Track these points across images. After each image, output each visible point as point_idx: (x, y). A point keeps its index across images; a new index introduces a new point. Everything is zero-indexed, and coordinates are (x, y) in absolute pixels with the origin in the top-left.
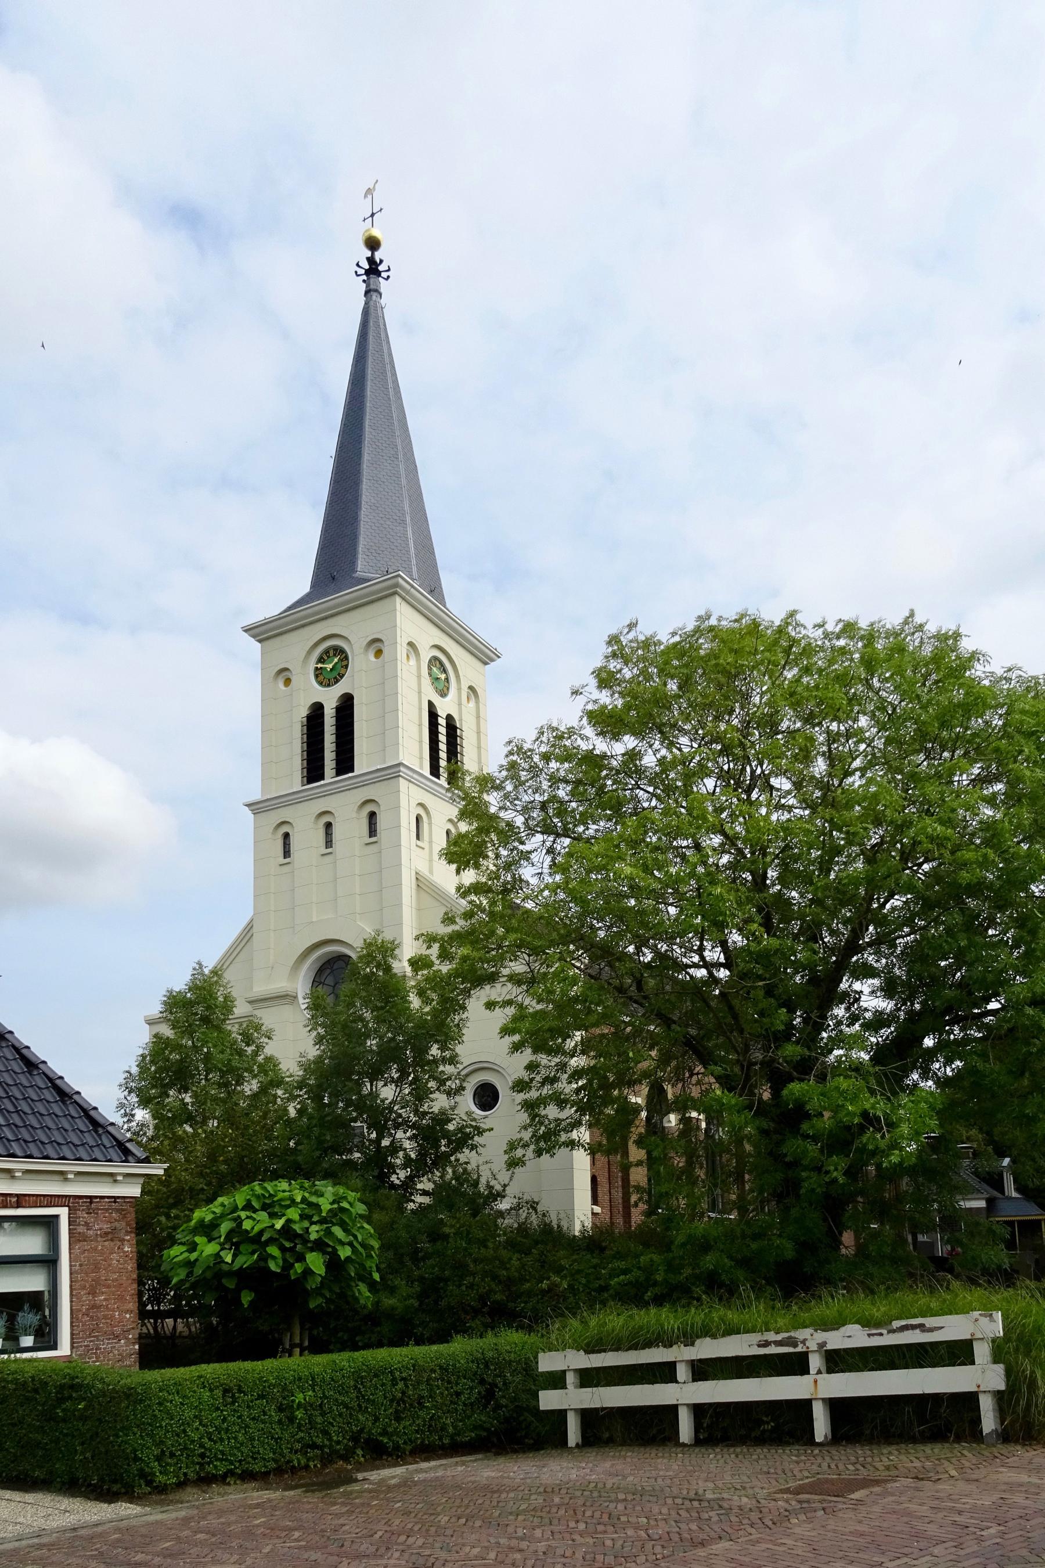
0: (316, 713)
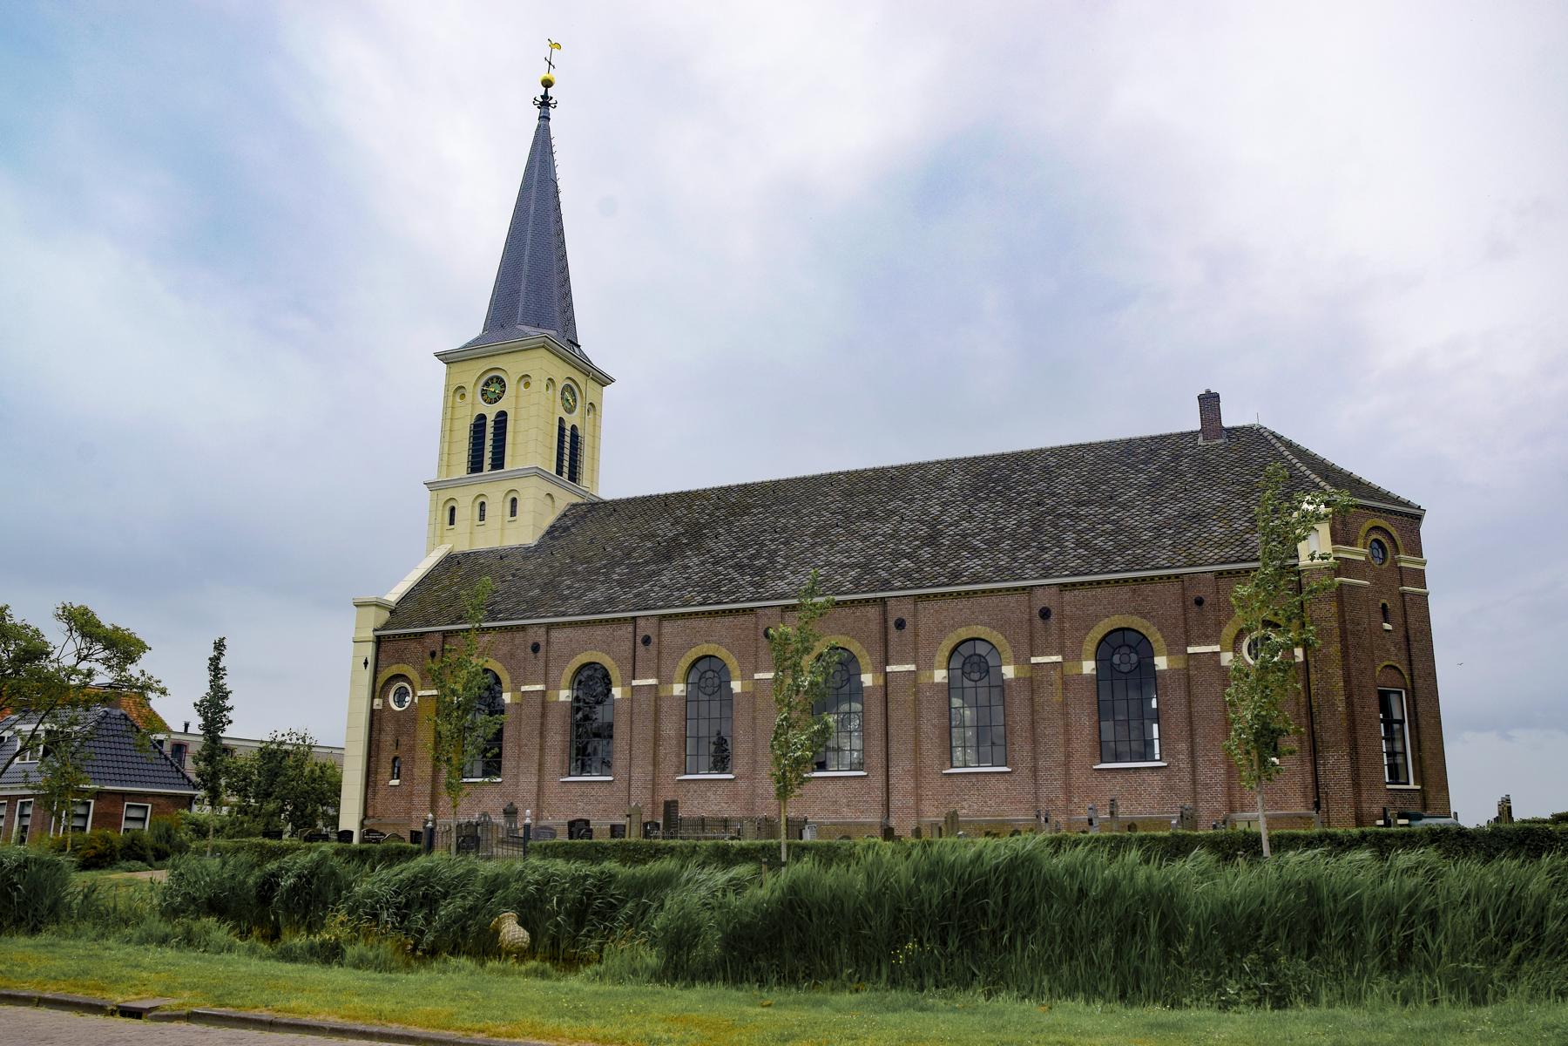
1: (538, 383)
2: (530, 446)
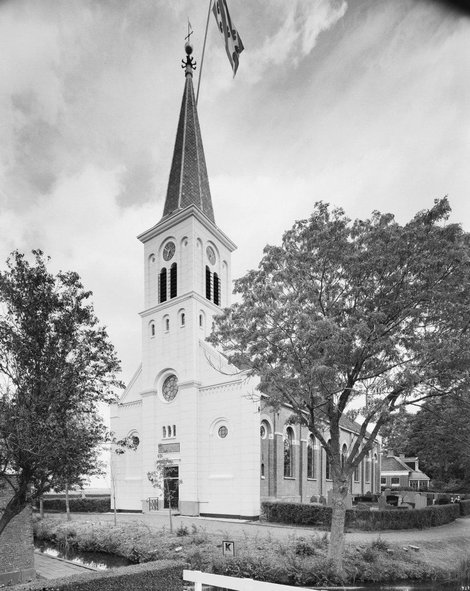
0: (164, 270)
1: (193, 242)
2: (191, 282)
